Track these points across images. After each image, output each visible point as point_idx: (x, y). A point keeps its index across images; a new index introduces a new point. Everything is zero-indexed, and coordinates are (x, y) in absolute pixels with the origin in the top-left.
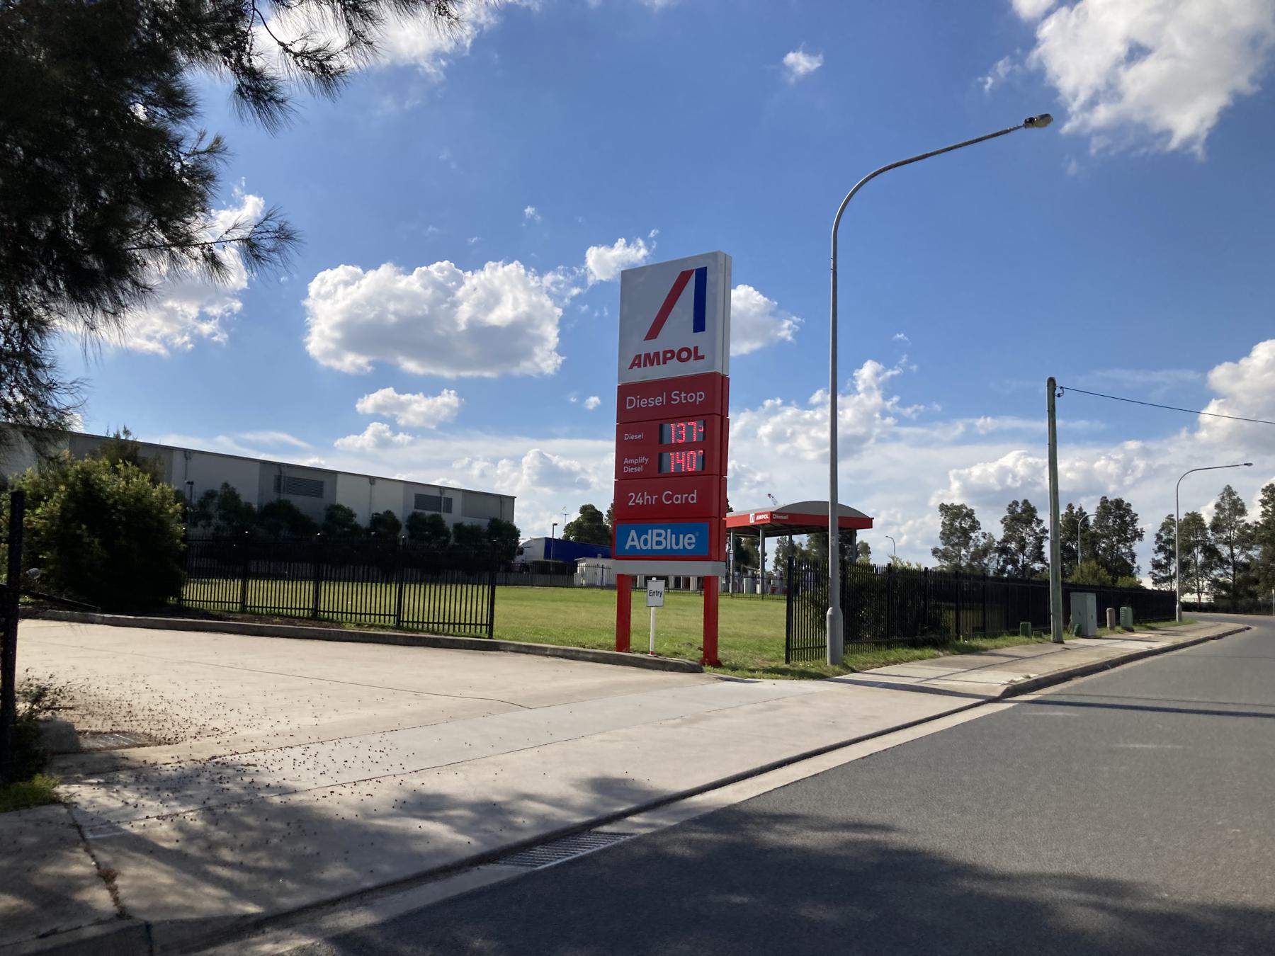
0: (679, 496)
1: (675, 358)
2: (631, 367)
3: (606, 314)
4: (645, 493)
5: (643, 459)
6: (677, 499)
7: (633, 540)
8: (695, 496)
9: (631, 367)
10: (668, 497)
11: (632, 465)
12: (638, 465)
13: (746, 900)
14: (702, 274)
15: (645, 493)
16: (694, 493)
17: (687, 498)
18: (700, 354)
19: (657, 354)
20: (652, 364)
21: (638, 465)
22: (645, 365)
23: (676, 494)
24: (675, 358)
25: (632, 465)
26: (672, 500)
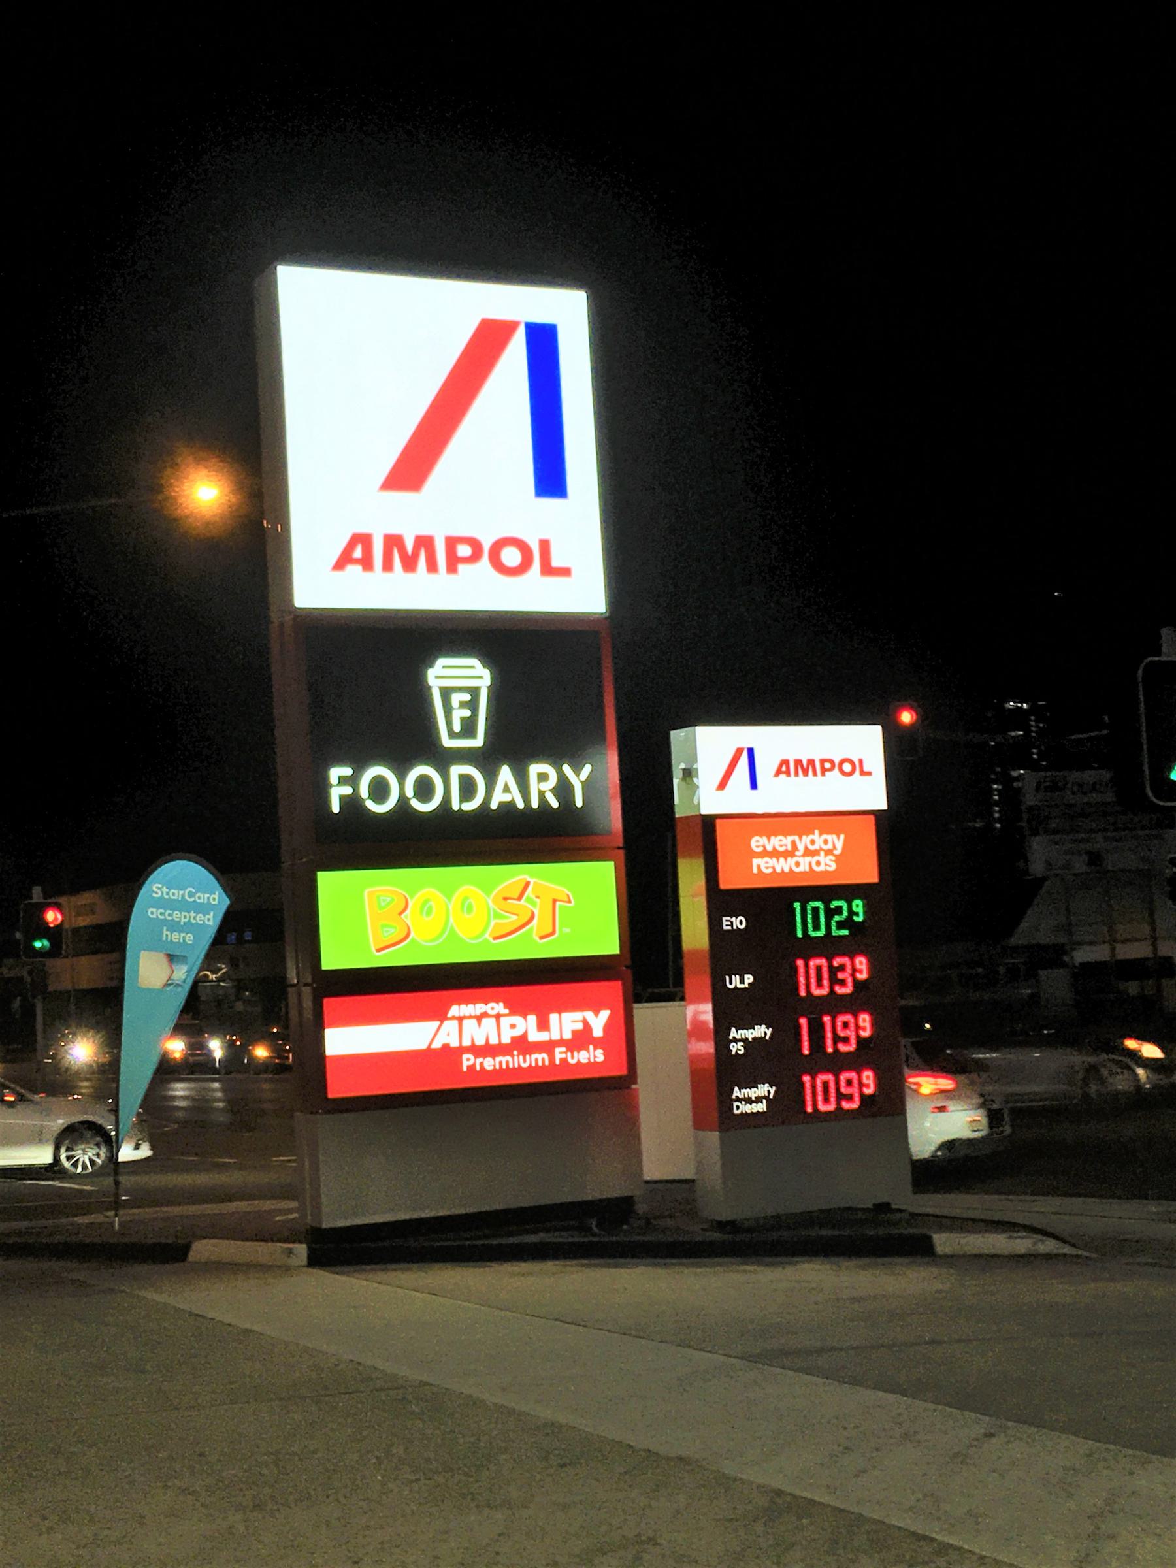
0: (202, 896)
1: (836, 769)
2: (340, 565)
3: (1151, 1051)
4: (165, 928)
5: (763, 1090)
6: (174, 894)
7: (506, 789)
8: (217, 897)
9: (340, 565)
10: (191, 895)
11: (749, 1101)
12: (759, 1100)
13: (974, 1056)
14: (751, 752)
15: (165, 928)
16: (215, 894)
17: (208, 898)
18: (556, 562)
19: (811, 762)
20: (410, 564)
21: (759, 1100)
22: (388, 566)
23: (199, 892)
24: (836, 769)
25: (749, 1101)
26: (170, 890)
